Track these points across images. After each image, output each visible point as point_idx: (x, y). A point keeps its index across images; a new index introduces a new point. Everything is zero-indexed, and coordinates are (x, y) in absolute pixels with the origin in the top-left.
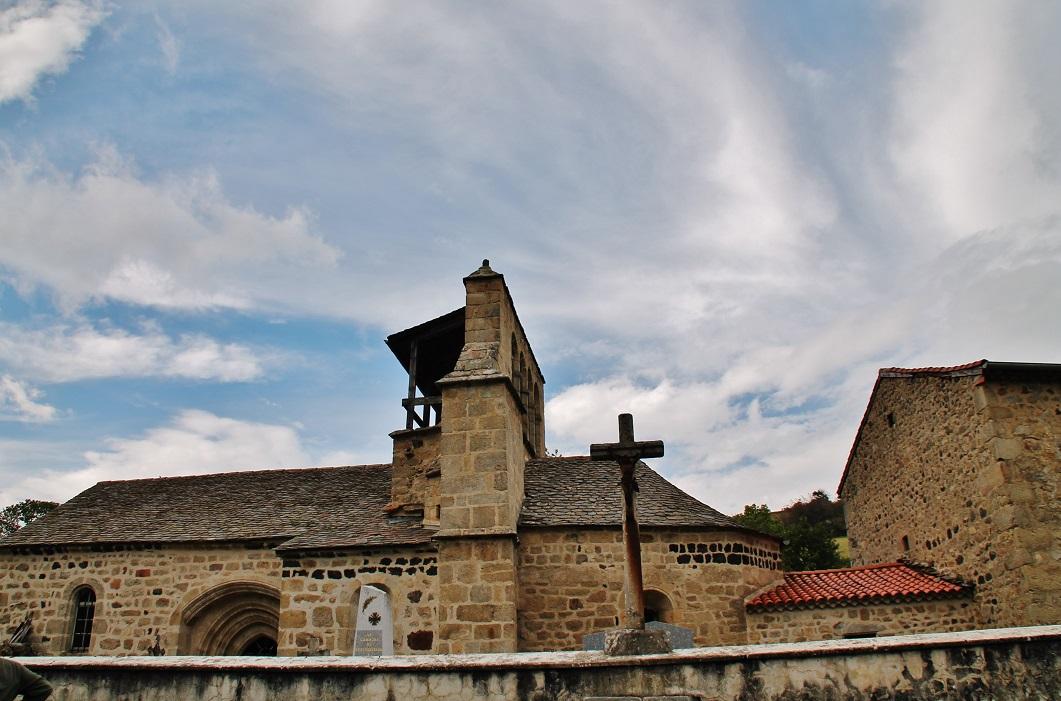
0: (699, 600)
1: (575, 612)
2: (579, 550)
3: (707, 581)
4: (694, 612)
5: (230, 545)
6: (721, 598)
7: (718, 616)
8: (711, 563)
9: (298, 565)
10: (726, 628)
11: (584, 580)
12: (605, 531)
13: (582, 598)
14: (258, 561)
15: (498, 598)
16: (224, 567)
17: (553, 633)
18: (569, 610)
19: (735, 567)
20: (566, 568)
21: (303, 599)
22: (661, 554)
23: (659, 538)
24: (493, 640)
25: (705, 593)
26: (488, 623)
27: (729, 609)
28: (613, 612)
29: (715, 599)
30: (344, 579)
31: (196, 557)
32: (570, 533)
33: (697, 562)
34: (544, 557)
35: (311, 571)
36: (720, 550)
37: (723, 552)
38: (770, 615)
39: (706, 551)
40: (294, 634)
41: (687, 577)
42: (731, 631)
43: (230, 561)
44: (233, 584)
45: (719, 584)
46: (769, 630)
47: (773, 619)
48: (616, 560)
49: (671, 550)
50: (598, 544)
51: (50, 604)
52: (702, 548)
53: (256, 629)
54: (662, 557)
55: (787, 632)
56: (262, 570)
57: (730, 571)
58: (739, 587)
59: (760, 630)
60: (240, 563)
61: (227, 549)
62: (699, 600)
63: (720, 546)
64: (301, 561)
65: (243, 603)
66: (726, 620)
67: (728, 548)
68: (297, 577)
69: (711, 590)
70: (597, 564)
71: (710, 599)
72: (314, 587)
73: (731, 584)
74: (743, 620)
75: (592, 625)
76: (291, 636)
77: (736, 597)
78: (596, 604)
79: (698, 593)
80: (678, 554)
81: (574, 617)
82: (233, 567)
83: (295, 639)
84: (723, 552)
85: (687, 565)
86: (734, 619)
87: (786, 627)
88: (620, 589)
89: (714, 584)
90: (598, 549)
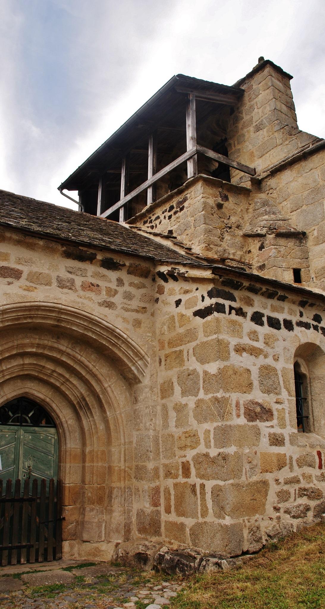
5: (41, 243)
9: (233, 299)
14: (83, 279)
16: (24, 275)
21: (244, 350)
30: (284, 331)
35: (250, 311)
40: (241, 402)
43: (35, 269)
44: (38, 308)
51: (203, 297)
53: (19, 383)
56: (89, 294)
60: (54, 275)
61: (31, 247)
64: (236, 294)
65: (27, 341)
68: (234, 316)
72: (254, 335)
76: (238, 405)
82: (37, 279)
83: (242, 411)
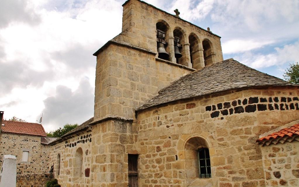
0: (226, 140)
1: (158, 153)
2: (159, 119)
3: (231, 127)
4: (222, 149)
6: (241, 137)
7: (240, 150)
8: (234, 114)
10: (246, 158)
11: (161, 135)
12: (169, 106)
13: (161, 146)
15: (106, 152)
17: (151, 165)
18: (156, 153)
19: (251, 114)
20: (154, 130)
22: (201, 113)
23: (199, 104)
24: (104, 173)
25: (230, 135)
26: (103, 164)
27: (248, 144)
28: (174, 153)
29: (237, 138)
31: (187, 105)
32: (154, 110)
33: (224, 115)
34: (146, 125)
36: (239, 104)
37: (242, 105)
38: (277, 146)
39: (230, 106)
41: (217, 126)
42: (250, 159)
45: (240, 128)
46: (277, 158)
47: (279, 149)
48: (175, 122)
49: (207, 110)
50: (166, 114)
52: (227, 105)
54: (201, 115)
55: (290, 159)
57: (247, 118)
58: (254, 128)
59: (271, 158)
61: (248, 91)
62: (226, 140)
63: (239, 101)
66: (246, 152)
67: (245, 102)
69: (234, 132)
70: (166, 125)
71: (233, 138)
73: (249, 126)
74: (259, 151)
75: (166, 160)
77: (253, 135)
78: (167, 148)
79: (225, 135)
80: (212, 112)
81: (158, 157)
84: (242, 105)
85: (217, 118)
86: (253, 151)
87: (289, 155)
88: (177, 138)
89: (235, 128)
90: (166, 117)
